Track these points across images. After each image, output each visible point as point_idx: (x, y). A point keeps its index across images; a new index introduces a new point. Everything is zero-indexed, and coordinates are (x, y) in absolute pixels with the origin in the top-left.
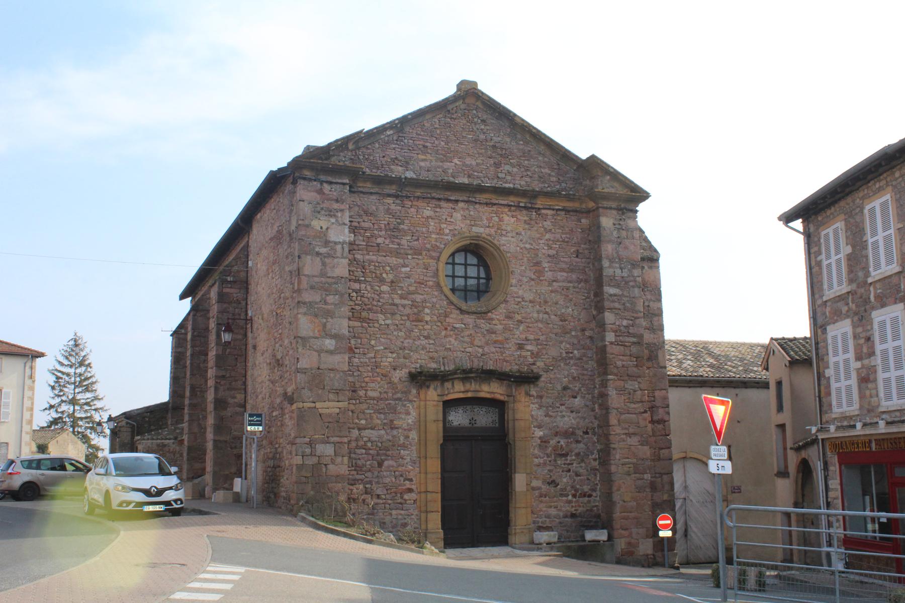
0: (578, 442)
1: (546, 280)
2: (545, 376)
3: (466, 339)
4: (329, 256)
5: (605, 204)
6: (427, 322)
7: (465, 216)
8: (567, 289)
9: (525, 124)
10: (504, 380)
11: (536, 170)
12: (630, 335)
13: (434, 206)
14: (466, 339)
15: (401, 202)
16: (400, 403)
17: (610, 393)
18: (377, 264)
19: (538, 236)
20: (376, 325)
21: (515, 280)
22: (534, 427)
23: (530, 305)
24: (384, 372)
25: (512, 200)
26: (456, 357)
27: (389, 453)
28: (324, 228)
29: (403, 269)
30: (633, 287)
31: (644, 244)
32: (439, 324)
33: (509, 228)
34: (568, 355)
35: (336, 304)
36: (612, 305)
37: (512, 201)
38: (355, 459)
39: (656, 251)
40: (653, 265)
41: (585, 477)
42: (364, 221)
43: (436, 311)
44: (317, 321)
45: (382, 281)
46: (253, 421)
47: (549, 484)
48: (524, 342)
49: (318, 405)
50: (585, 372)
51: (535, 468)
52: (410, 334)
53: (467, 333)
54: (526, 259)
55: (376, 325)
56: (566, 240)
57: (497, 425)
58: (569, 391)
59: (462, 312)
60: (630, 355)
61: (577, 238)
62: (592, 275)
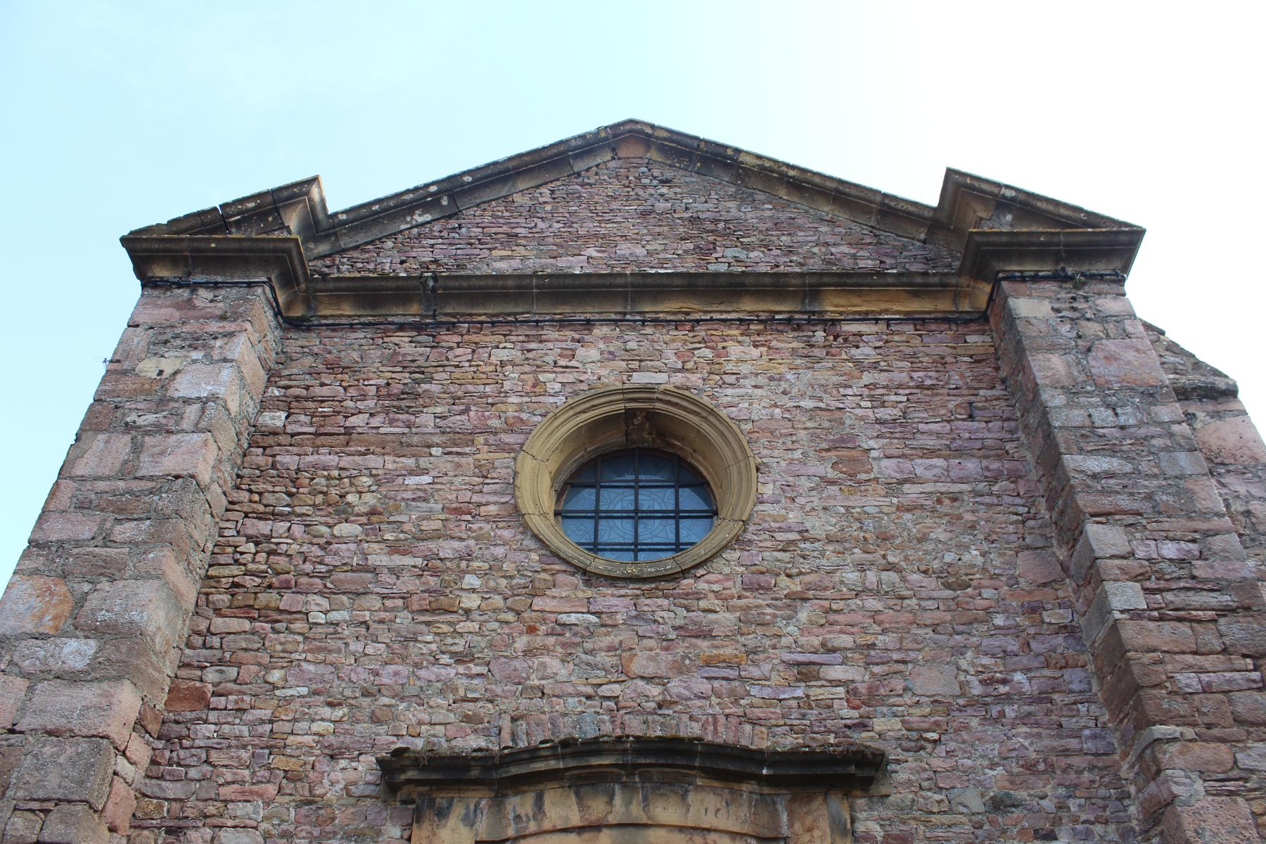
1: (876, 479)
2: (912, 764)
3: (604, 658)
6: (467, 612)
7: (610, 353)
8: (955, 500)
9: (767, 164)
10: (740, 777)
11: (816, 250)
12: (1197, 584)
13: (521, 338)
14: (604, 658)
15: (431, 339)
17: (1176, 789)
19: (835, 379)
21: (771, 486)
23: (831, 548)
24: (292, 764)
25: (749, 306)
26: (565, 715)
29: (411, 481)
30: (1167, 449)
32: (510, 617)
34: (990, 689)
35: (137, 544)
36: (1106, 503)
42: (322, 385)
43: (504, 582)
44: (62, 589)
48: (814, 658)
50: (1073, 743)
52: (406, 648)
56: (928, 382)
58: (1017, 813)
59: (590, 577)
60: (1225, 651)
61: (962, 376)
62: (1029, 456)
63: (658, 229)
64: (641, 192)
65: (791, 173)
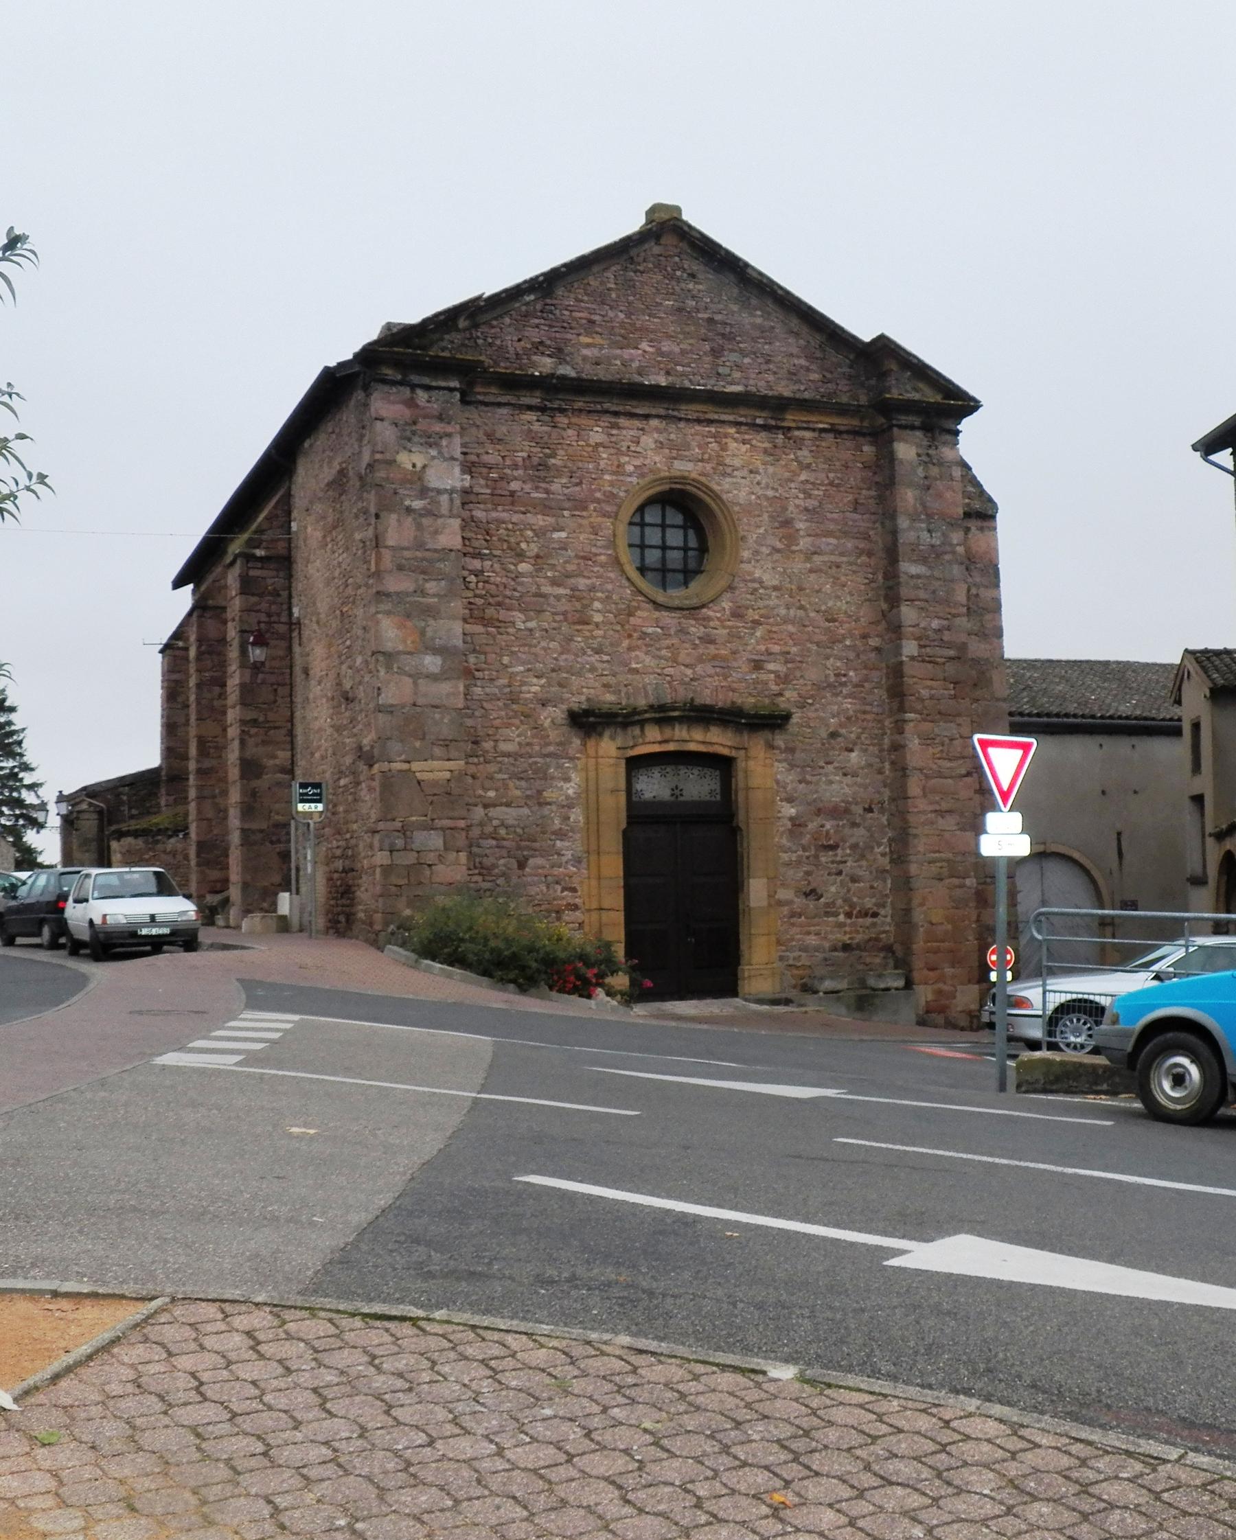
0: (854, 825)
4: (429, 513)
5: (904, 419)
6: (597, 625)
12: (943, 644)
16: (554, 761)
18: (510, 526)
19: (787, 475)
20: (511, 630)
22: (781, 800)
25: (743, 414)
27: (536, 845)
28: (419, 465)
29: (556, 535)
31: (970, 489)
32: (618, 628)
33: (737, 462)
37: (745, 416)
38: (480, 856)
39: (990, 500)
40: (985, 524)
41: (868, 885)
44: (409, 624)
45: (521, 556)
46: (306, 794)
47: (806, 895)
49: (415, 766)
50: (868, 708)
51: (783, 870)
53: (668, 642)
54: (766, 516)
55: (511, 630)
57: (718, 797)
58: (840, 739)
60: (945, 680)
63: (687, 329)
64: (674, 283)
65: (780, 292)
